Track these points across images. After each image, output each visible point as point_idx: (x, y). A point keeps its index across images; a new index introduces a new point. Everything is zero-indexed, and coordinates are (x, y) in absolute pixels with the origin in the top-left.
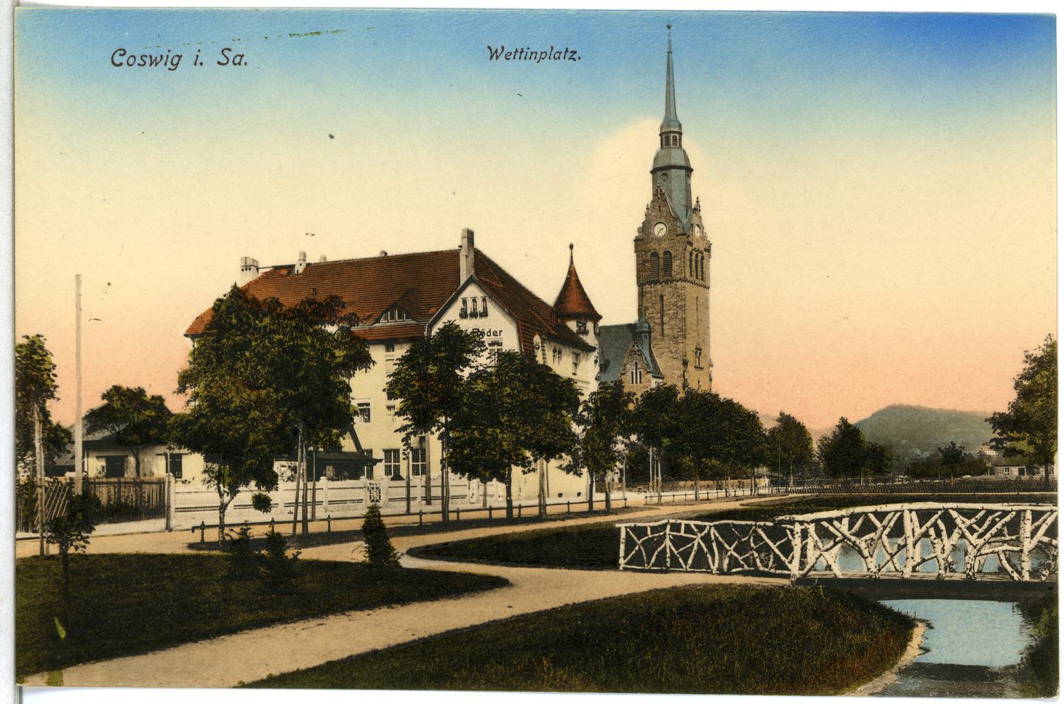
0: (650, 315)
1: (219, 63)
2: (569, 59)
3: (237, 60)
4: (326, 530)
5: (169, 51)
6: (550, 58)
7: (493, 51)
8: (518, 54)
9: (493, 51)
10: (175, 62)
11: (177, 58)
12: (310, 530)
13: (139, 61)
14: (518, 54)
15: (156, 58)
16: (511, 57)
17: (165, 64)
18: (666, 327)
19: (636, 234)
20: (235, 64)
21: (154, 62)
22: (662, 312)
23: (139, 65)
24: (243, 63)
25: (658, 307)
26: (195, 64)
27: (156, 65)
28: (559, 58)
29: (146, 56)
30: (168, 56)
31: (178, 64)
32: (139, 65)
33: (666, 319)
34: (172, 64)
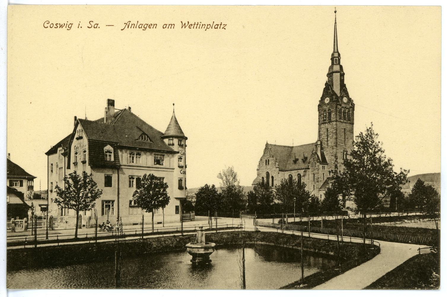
0: (323, 138)
1: (88, 27)
2: (223, 28)
3: (95, 26)
4: (25, 246)
5: (80, 22)
6: (212, 28)
7: (183, 24)
8: (196, 26)
9: (183, 24)
10: (70, 26)
11: (71, 25)
12: (97, 236)
13: (55, 26)
14: (196, 26)
15: (62, 25)
16: (192, 27)
17: (66, 27)
18: (329, 142)
19: (318, 103)
20: (139, 28)
21: (61, 26)
22: (328, 136)
23: (55, 27)
24: (98, 27)
25: (326, 134)
26: (78, 27)
27: (62, 27)
28: (217, 28)
29: (58, 24)
30: (67, 24)
31: (71, 27)
32: (55, 27)
33: (329, 139)
34: (69, 27)
